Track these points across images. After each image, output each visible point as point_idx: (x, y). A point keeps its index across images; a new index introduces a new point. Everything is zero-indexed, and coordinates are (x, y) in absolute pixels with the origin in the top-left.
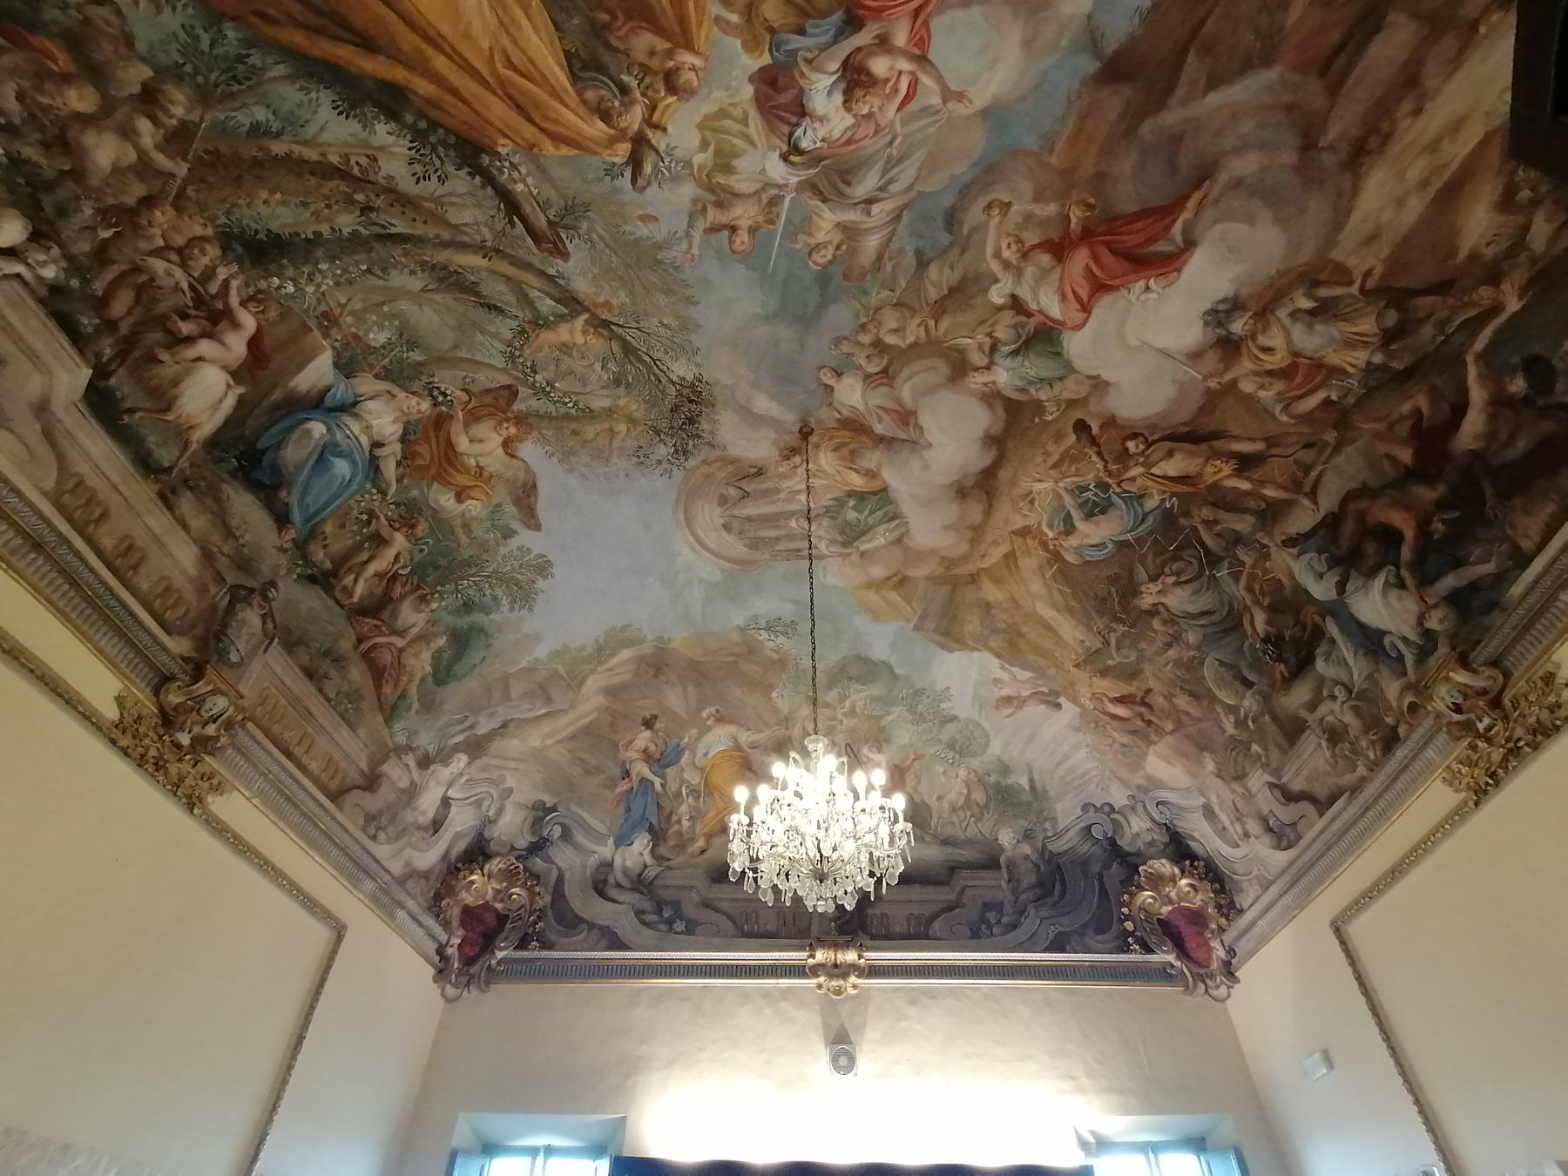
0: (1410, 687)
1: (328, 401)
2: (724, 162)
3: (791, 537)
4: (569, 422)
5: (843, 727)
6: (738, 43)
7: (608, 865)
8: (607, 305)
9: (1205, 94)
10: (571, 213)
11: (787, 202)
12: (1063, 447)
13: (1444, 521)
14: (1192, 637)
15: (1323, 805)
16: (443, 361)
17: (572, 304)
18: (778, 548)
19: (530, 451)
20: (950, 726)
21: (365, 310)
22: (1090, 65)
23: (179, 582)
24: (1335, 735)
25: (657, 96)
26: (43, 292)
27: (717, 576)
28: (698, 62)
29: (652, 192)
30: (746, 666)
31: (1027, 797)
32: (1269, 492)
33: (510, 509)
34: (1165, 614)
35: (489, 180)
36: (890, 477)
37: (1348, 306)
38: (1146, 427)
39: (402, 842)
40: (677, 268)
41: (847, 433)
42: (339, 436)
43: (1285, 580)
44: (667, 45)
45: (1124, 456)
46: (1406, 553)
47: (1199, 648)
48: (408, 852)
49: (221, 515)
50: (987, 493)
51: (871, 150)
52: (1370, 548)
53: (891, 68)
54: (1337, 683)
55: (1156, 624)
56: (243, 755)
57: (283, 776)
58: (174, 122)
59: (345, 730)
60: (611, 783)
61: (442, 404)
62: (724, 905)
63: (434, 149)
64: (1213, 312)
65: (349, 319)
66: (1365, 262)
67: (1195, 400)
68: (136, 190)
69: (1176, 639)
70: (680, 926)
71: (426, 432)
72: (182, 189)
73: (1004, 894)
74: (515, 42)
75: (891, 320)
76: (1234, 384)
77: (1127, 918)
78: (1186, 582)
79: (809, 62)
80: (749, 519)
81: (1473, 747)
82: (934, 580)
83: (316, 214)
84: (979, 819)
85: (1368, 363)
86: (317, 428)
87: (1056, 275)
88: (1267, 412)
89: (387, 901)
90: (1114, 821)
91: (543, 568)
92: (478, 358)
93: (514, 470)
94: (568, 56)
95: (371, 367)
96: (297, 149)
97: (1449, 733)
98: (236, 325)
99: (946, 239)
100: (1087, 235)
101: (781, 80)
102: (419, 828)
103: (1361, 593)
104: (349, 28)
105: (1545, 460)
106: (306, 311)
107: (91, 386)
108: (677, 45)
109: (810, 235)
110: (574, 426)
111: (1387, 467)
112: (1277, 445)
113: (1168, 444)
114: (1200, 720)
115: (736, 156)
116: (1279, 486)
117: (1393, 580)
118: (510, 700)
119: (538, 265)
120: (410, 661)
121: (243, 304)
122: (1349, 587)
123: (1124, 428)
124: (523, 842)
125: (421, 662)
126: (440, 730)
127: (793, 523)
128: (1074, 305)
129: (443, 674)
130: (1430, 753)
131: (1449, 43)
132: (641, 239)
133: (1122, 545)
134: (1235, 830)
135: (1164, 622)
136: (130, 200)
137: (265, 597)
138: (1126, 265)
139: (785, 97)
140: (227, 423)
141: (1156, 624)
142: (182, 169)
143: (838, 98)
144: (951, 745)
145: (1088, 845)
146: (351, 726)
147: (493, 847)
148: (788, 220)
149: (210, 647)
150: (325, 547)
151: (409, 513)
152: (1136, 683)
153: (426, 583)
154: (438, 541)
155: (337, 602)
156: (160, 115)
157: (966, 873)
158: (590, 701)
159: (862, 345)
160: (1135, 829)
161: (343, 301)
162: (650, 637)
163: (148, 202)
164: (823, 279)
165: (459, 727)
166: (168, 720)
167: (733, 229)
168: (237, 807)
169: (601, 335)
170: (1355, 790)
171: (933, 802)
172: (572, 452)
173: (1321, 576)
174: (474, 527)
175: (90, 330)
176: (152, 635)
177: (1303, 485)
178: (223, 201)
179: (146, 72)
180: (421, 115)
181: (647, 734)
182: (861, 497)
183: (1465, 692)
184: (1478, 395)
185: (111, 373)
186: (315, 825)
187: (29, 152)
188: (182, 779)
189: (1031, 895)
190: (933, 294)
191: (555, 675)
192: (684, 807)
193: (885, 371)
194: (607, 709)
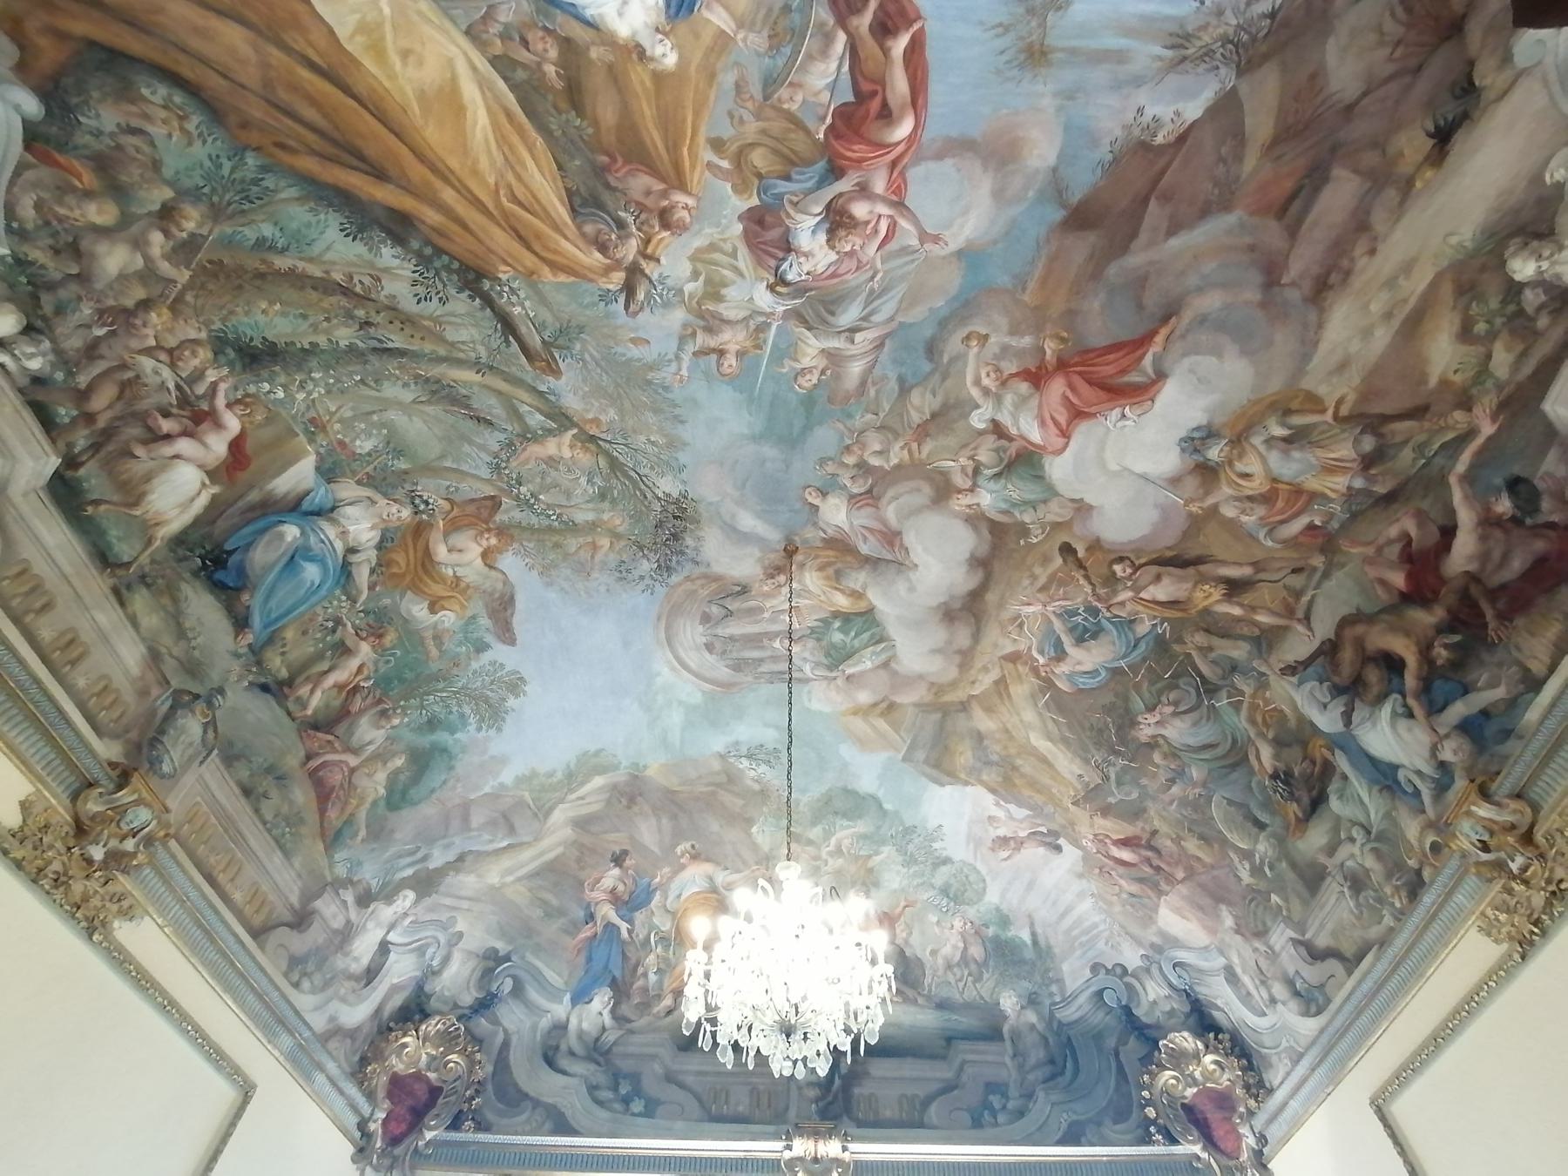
0: (1431, 825)
1: (305, 506)
2: (714, 291)
3: (775, 659)
4: (552, 536)
5: (828, 869)
6: (729, 186)
7: (561, 1027)
8: (596, 421)
9: (1166, 240)
10: (564, 336)
11: (774, 328)
12: (1050, 570)
13: (1446, 646)
14: (1195, 773)
15: (1351, 962)
16: (430, 469)
17: (561, 419)
18: (761, 669)
19: (510, 562)
20: (944, 869)
21: (354, 418)
22: (1058, 215)
23: (121, 682)
24: (1357, 883)
26: (24, 381)
27: (697, 698)
28: (691, 202)
29: (644, 317)
30: (726, 797)
31: (1029, 954)
32: (1263, 618)
33: (485, 621)
34: (1166, 748)
35: (488, 302)
36: (875, 597)
37: (1323, 432)
38: (1133, 551)
39: (330, 992)
40: (666, 389)
41: (831, 553)
42: (313, 540)
43: (1287, 711)
44: (661, 186)
45: (1111, 580)
46: (1410, 681)
47: (1204, 785)
48: (335, 1006)
49: (176, 618)
50: (975, 615)
51: (853, 283)
52: (1373, 675)
54: (1354, 823)
55: (1157, 757)
56: (162, 876)
57: (202, 904)
58: (184, 235)
59: (278, 857)
60: (572, 929)
61: (422, 512)
62: (689, 1080)
63: (437, 274)
64: (1188, 439)
65: (337, 426)
66: (1338, 391)
67: (1180, 524)
68: (140, 293)
69: (1178, 775)
70: (638, 1106)
73: (1007, 1071)
74: (519, 178)
76: (1214, 510)
77: (1149, 1102)
78: (1185, 712)
79: (795, 204)
80: (732, 639)
81: (1510, 891)
83: (315, 328)
84: (978, 979)
85: (1349, 488)
86: (291, 532)
87: (1034, 402)
88: (1251, 536)
89: (305, 1061)
90: (1129, 987)
91: (515, 685)
92: (465, 468)
93: (492, 582)
94: (570, 194)
96: (301, 265)
97: (1478, 874)
98: (219, 425)
99: (927, 367)
100: (1062, 365)
101: (769, 219)
102: (351, 977)
103: (1368, 724)
104: (361, 157)
105: (1542, 578)
106: (294, 417)
107: (57, 476)
109: (796, 360)
110: (556, 538)
111: (1380, 591)
112: (1264, 570)
113: (1154, 569)
114: (1213, 867)
115: (725, 285)
117: (1400, 710)
118: (470, 830)
120: (361, 781)
121: (229, 406)
122: (1356, 717)
123: (1110, 551)
124: (467, 999)
126: (387, 862)
127: (777, 644)
128: (1053, 430)
129: (398, 797)
130: (1459, 898)
131: (1391, 194)
132: (631, 360)
133: (1116, 672)
134: (1260, 996)
135: (1165, 756)
136: (129, 303)
137: (210, 704)
138: (1101, 393)
139: (774, 234)
140: (197, 522)
141: (1157, 757)
142: (183, 276)
144: (945, 891)
145: (1100, 1015)
146: (287, 854)
147: (434, 1004)
149: (141, 755)
150: (283, 654)
151: (377, 624)
152: (1140, 824)
153: (388, 697)
155: (289, 714)
156: (174, 230)
157: (963, 1045)
158: (557, 834)
159: (847, 466)
160: (1152, 997)
161: (333, 409)
162: (625, 763)
163: (145, 305)
164: (809, 401)
165: (409, 860)
166: (81, 830)
167: (721, 353)
168: (145, 937)
169: (587, 450)
170: (1383, 943)
171: (926, 956)
173: (1325, 706)
174: (446, 640)
175: (67, 420)
176: (78, 734)
177: (1295, 610)
178: (222, 308)
179: (168, 194)
180: (428, 242)
181: (616, 872)
182: (846, 618)
183: (1490, 828)
184: (1466, 517)
185: (82, 464)
186: (232, 964)
187: (37, 254)
188: (86, 898)
189: (1039, 1074)
190: (916, 418)
191: (521, 803)
193: (870, 491)
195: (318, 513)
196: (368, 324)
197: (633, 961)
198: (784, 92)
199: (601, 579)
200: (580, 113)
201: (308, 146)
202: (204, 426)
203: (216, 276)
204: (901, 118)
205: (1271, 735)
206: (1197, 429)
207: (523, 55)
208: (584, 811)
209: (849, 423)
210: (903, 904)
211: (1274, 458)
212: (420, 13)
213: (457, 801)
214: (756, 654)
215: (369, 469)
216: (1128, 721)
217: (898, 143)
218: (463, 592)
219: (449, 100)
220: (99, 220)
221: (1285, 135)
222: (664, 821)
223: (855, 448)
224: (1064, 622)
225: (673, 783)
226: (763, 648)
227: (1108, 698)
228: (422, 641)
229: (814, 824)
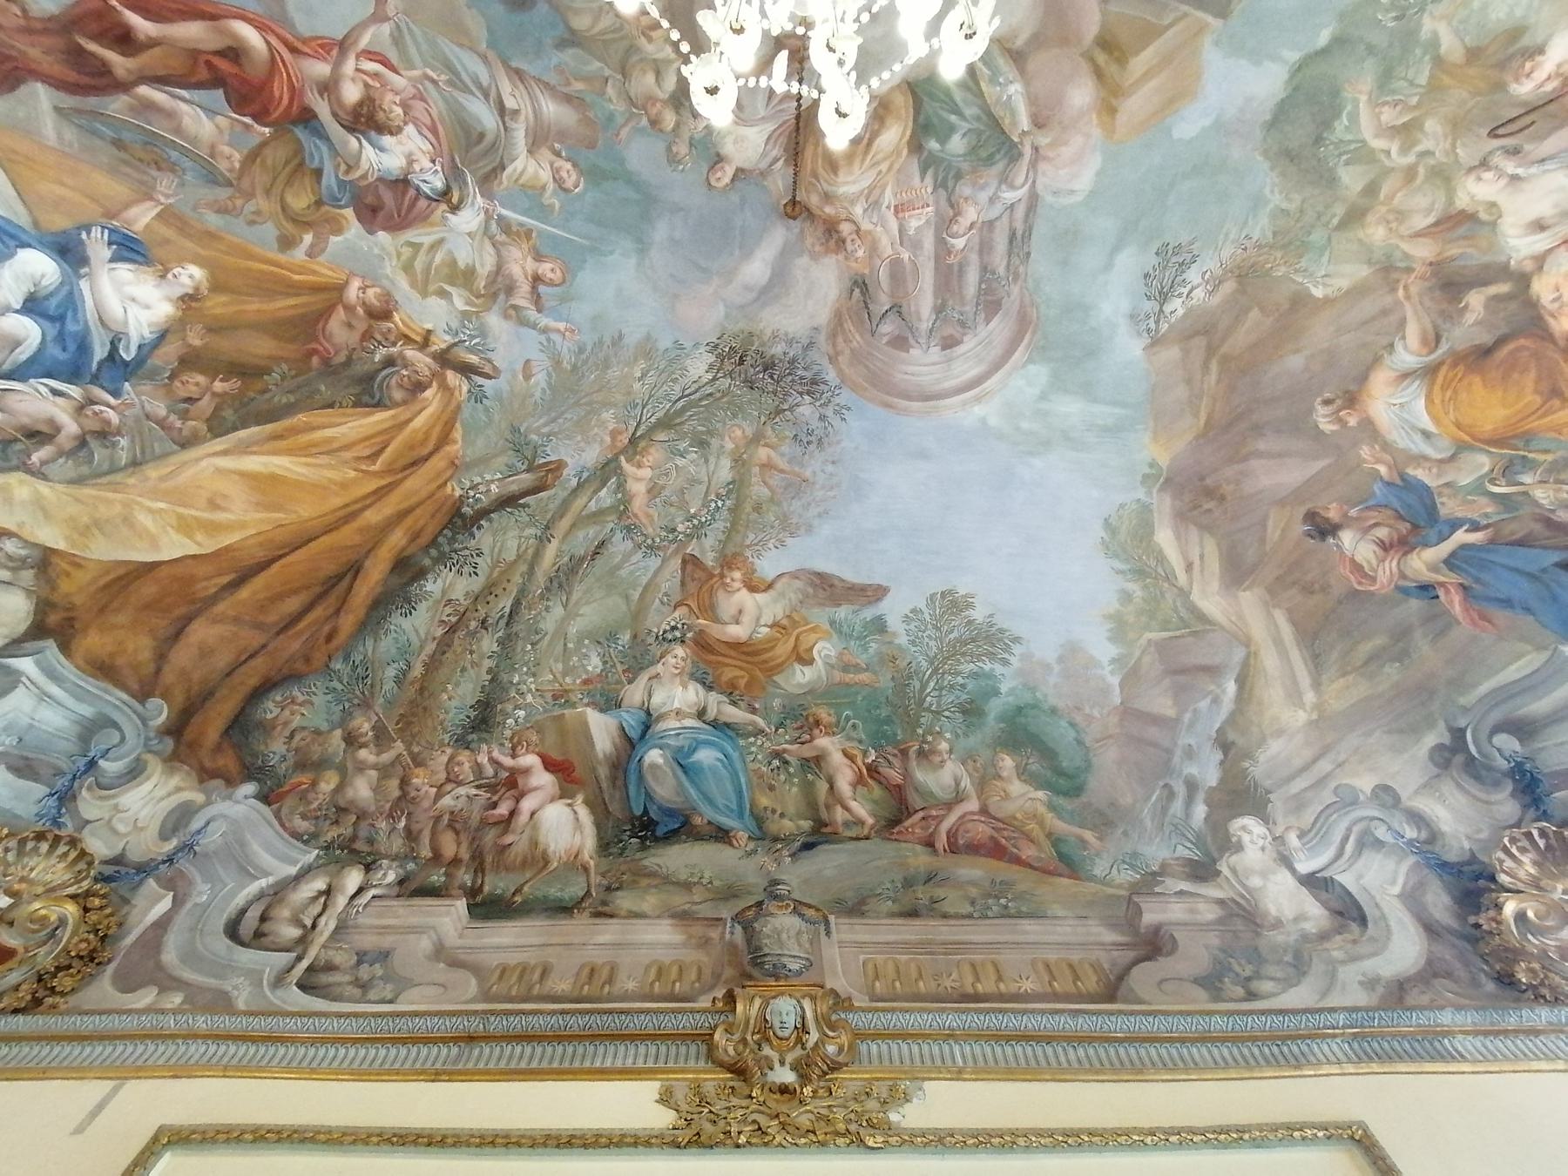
1: (634, 734)
2: (465, 277)
6: (334, 239)
8: (614, 434)
11: (504, 212)
16: (638, 614)
17: (607, 470)
18: (1001, 270)
25: (395, 332)
27: (1039, 373)
30: (1241, 339)
33: (842, 612)
35: (484, 513)
40: (581, 350)
42: (672, 742)
44: (340, 309)
49: (667, 881)
51: (441, 103)
53: (353, 80)
59: (1028, 926)
60: (1439, 622)
65: (568, 680)
68: (394, 783)
71: (709, 663)
72: (411, 753)
79: (349, 169)
80: (939, 310)
83: (474, 664)
86: (654, 756)
91: (952, 604)
92: (644, 580)
95: (619, 682)
96: (423, 657)
98: (526, 771)
101: (369, 200)
104: (340, 577)
107: (471, 908)
108: (340, 300)
109: (543, 188)
110: (748, 508)
115: (454, 262)
118: (1177, 720)
119: (566, 494)
121: (514, 756)
125: (1021, 796)
127: (959, 243)
132: (549, 384)
136: (397, 793)
137: (776, 897)
139: (388, 197)
140: (598, 825)
142: (399, 746)
143: (387, 140)
148: (525, 213)
150: (782, 815)
151: (801, 718)
154: (852, 705)
156: (363, 740)
158: (1254, 619)
159: (678, 125)
162: (1141, 494)
163: (404, 782)
164: (594, 175)
167: (537, 279)
168: (939, 1103)
178: (435, 729)
179: (338, 733)
181: (1347, 538)
187: (332, 834)
191: (1161, 647)
192: (1540, 494)
194: (1271, 591)
195: (647, 727)
196: (484, 622)
197: (1538, 527)
198: (223, 166)
199: (815, 465)
200: (268, 371)
201: (328, 618)
202: (520, 781)
203: (409, 724)
204: (234, 36)
207: (206, 405)
208: (1214, 564)
209: (620, 120)
212: (162, 479)
213: (1114, 720)
214: (972, 276)
215: (620, 668)
217: (268, 42)
219: (266, 487)
220: (332, 786)
222: (1262, 445)
223: (653, 111)
225: (1188, 428)
226: (962, 267)
229: (1332, 181)
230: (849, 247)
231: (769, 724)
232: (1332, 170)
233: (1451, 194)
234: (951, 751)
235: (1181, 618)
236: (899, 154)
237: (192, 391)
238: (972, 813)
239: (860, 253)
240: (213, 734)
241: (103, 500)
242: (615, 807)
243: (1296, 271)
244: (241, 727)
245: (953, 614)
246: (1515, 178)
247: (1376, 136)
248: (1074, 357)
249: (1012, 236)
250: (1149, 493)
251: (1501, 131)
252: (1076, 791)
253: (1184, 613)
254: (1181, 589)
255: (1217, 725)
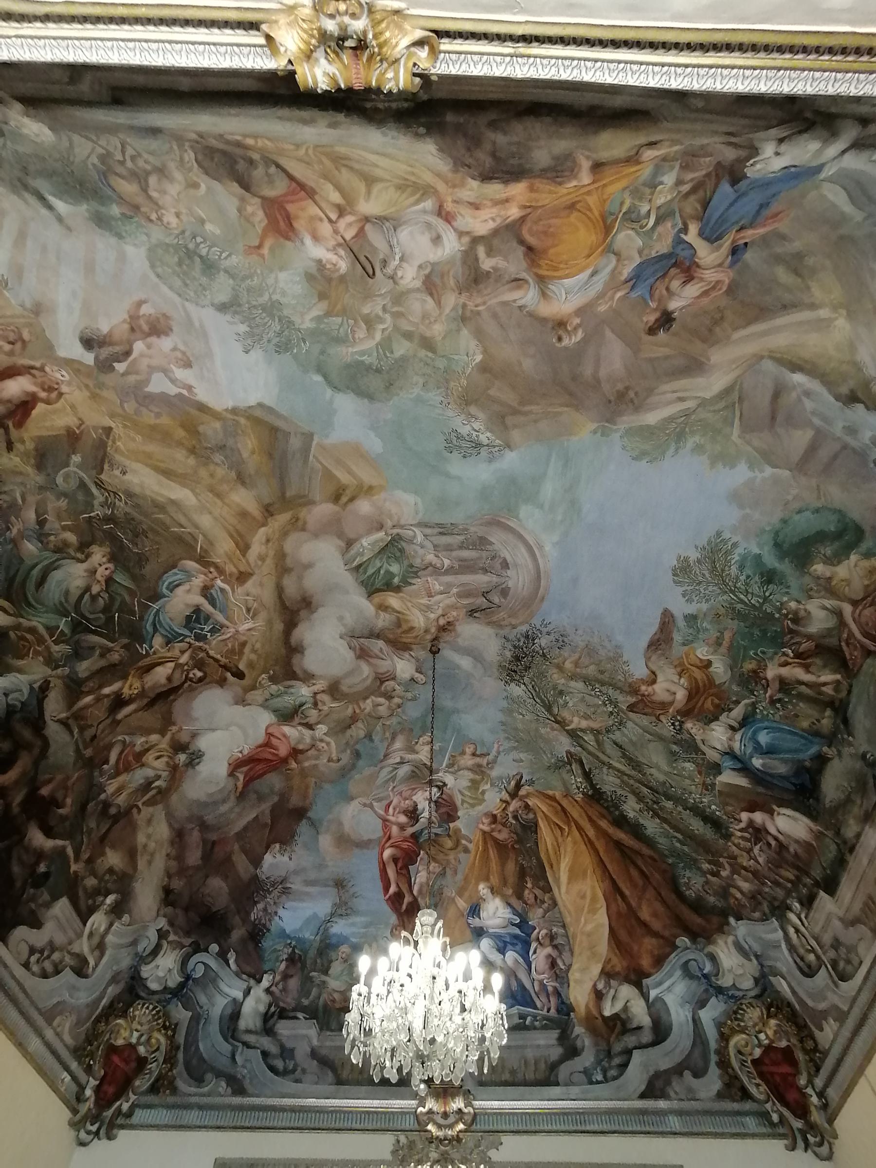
1: (739, 766)
2: (475, 785)
4: (603, 680)
5: (381, 302)
8: (553, 729)
12: (245, 658)
14: (30, 548)
16: (661, 738)
17: (573, 734)
19: (639, 670)
27: (524, 511)
30: (510, 397)
32: (88, 699)
33: (677, 637)
36: (368, 607)
38: (196, 689)
40: (508, 738)
43: (20, 663)
55: (71, 537)
75: (383, 710)
78: (82, 596)
80: (485, 571)
82: (305, 501)
86: (757, 762)
98: (751, 823)
99: (358, 747)
101: (446, 817)
106: (715, 796)
110: (600, 677)
111: (47, 776)
113: (176, 683)
116: (87, 707)
118: (818, 431)
120: (857, 589)
127: (447, 562)
133: (156, 596)
135: (66, 544)
139: (443, 810)
143: (420, 807)
144: (210, 267)
151: (752, 680)
152: (30, 445)
155: (849, 692)
167: (474, 754)
172: (610, 659)
173: (6, 695)
177: (75, 720)
180: (610, 813)
181: (674, 305)
182: (389, 586)
190: (360, 724)
191: (747, 428)
192: (660, 200)
193: (382, 682)
199: (579, 641)
205: (12, 634)
206: (198, 763)
207: (538, 892)
209: (399, 719)
210: (265, 251)
211: (150, 773)
216: (117, 557)
218: (681, 664)
219: (573, 875)
221: (228, 859)
224: (217, 622)
227: (148, 570)
228: (730, 648)
229: (404, 359)
230: (451, 619)
231: (749, 698)
232: (396, 361)
233: (410, 291)
234: (799, 602)
235: (726, 407)
236: (402, 597)
237: (532, 897)
238: (853, 612)
239: (455, 614)
240: (699, 920)
241: (580, 943)
242: (786, 796)
243: (463, 373)
244: (698, 906)
245: (690, 572)
246: (402, 259)
247: (373, 338)
248: (516, 491)
249: (441, 534)
250: (616, 431)
251: (371, 272)
252: (859, 533)
253: (722, 404)
254: (699, 406)
255: (832, 399)
